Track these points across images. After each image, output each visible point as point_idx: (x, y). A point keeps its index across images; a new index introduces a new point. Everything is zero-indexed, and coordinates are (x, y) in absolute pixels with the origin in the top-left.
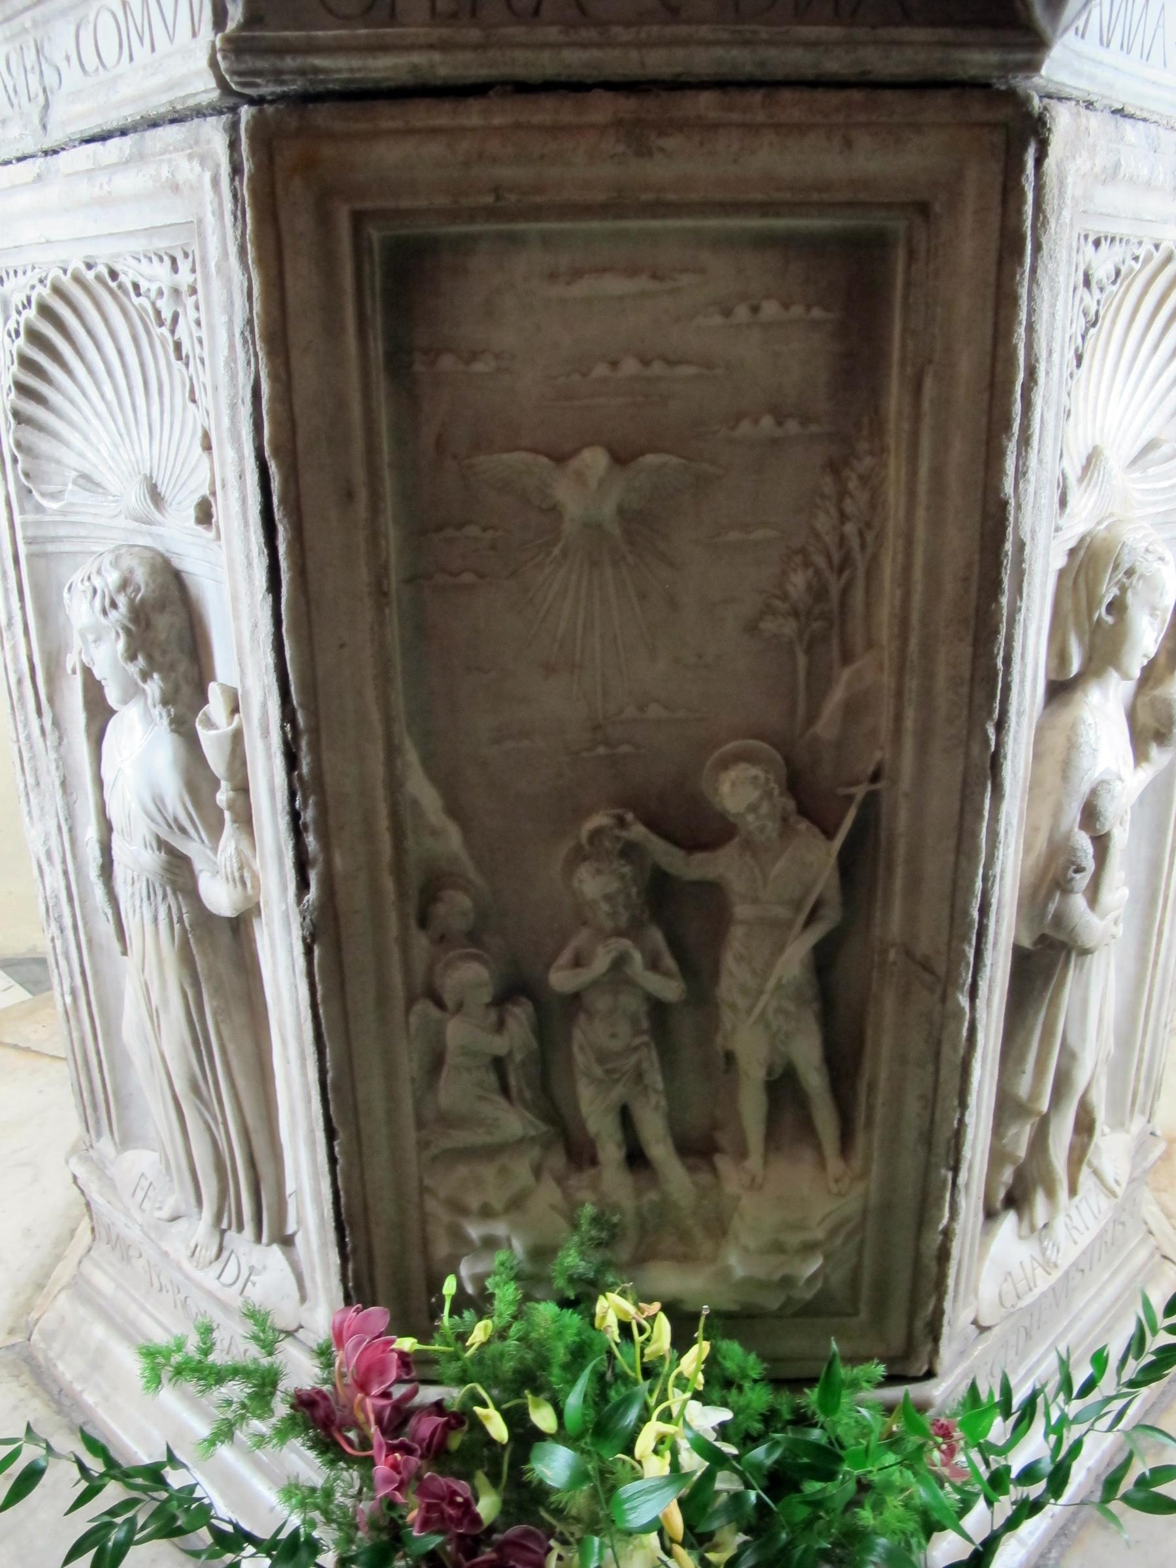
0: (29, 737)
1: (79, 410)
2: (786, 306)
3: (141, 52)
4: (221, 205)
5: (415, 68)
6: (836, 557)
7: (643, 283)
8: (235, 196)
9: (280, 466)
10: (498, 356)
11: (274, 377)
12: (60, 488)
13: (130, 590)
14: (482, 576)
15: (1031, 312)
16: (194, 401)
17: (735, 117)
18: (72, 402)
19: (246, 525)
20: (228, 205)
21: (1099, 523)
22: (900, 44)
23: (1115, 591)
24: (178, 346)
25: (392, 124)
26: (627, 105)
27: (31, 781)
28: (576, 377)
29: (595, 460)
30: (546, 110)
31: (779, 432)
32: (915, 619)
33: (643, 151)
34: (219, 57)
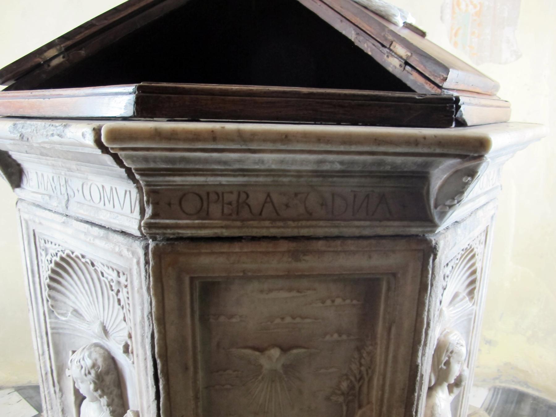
0: (49, 393)
1: (74, 288)
2: (344, 300)
3: (109, 206)
4: (140, 271)
5: (216, 233)
6: (358, 377)
7: (294, 294)
8: (146, 271)
9: (161, 361)
10: (241, 317)
11: (159, 332)
12: (65, 312)
13: (96, 368)
14: (232, 386)
15: (429, 305)
16: (125, 321)
17: (331, 249)
18: (71, 285)
19: (147, 375)
20: (143, 273)
21: (441, 334)
22: (389, 226)
23: (447, 358)
24: (119, 301)
25: (206, 251)
26: (292, 245)
27: (49, 407)
28: (269, 323)
29: (275, 353)
30: (263, 247)
31: (339, 339)
32: (385, 401)
33: (297, 260)
34: (142, 229)
